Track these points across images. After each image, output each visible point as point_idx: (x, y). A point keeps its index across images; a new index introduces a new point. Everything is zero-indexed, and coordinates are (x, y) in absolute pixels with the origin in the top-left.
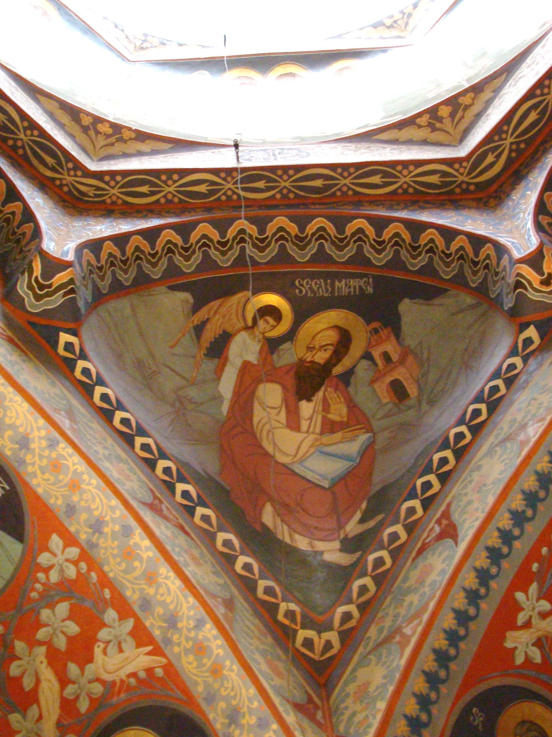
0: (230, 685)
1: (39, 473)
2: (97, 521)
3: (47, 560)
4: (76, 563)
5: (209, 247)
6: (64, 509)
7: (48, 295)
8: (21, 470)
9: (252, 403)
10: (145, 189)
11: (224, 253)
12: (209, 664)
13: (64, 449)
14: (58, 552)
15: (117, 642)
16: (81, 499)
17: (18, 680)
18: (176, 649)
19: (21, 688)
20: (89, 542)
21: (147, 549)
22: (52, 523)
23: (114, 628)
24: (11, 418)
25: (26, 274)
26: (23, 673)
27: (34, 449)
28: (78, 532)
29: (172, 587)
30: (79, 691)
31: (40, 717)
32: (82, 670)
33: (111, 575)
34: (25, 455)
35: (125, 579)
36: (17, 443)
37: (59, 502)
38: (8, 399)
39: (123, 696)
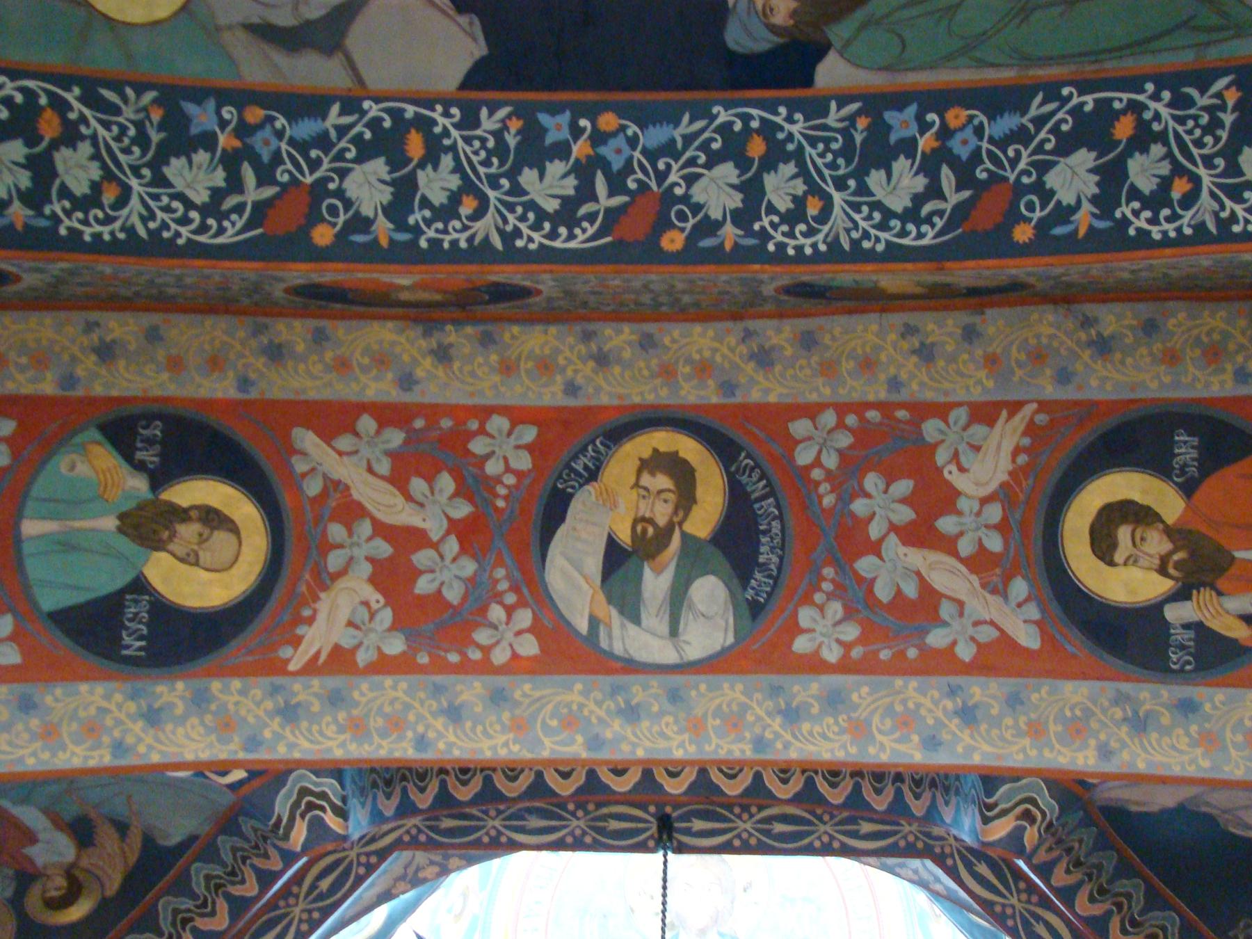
5: (197, 907)
6: (36, 699)
7: (296, 804)
8: (128, 687)
10: (325, 884)
11: (176, 912)
25: (339, 803)
34: (139, 707)
36: (161, 709)
37: (49, 699)
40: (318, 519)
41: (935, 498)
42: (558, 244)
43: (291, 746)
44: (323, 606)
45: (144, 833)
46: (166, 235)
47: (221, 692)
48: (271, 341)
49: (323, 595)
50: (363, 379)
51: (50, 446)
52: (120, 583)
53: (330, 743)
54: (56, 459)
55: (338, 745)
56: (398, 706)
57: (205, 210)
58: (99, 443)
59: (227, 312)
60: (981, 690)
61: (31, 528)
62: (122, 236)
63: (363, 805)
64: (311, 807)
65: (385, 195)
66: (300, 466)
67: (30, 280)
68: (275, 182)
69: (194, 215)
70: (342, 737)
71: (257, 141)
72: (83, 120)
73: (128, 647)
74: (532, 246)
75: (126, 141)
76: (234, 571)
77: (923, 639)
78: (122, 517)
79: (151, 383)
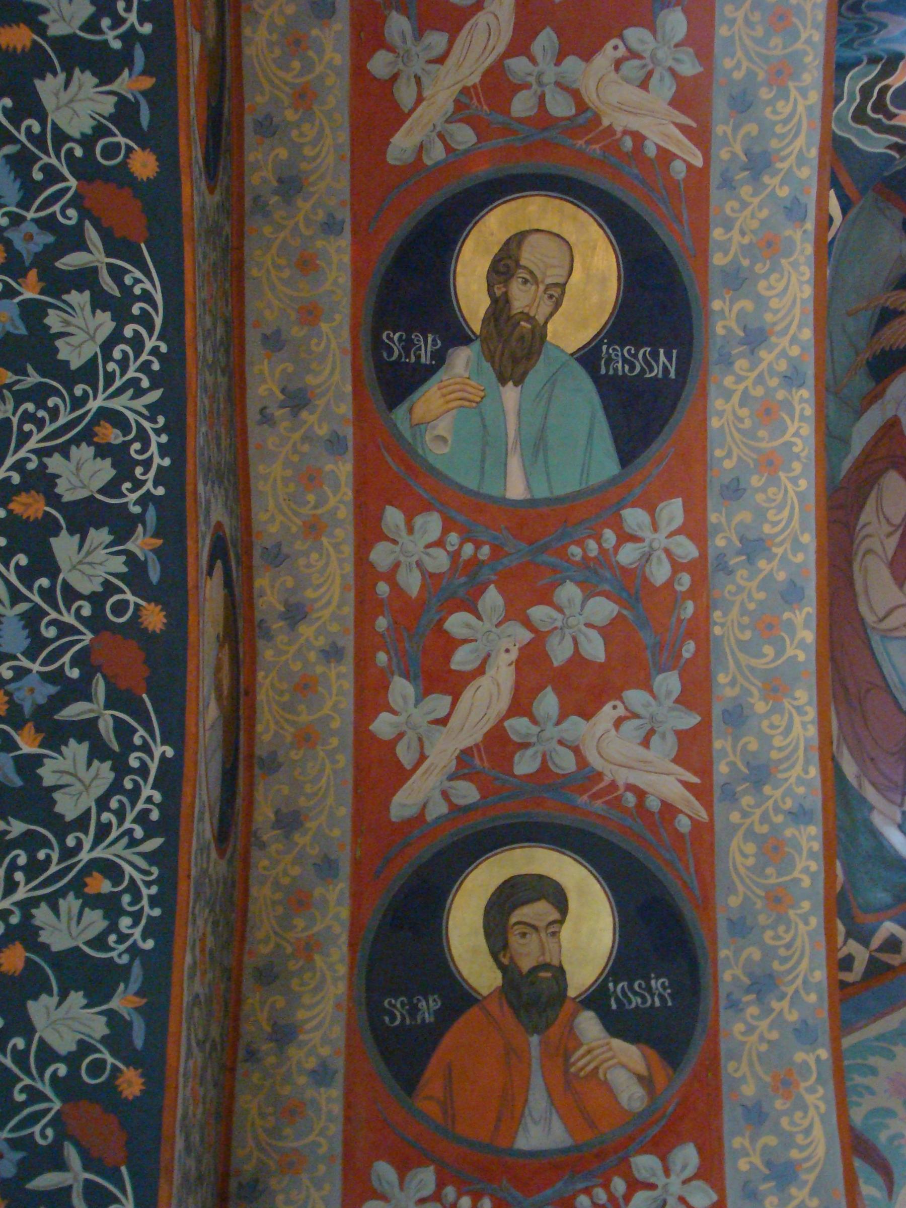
0: (788, 938)
1: (736, 398)
2: (761, 540)
3: (639, 526)
4: (677, 567)
7: (878, 127)
8: (715, 371)
9: (872, 488)
12: (773, 881)
13: (802, 401)
14: (665, 530)
15: (648, 727)
16: (763, 489)
17: (451, 644)
18: (735, 817)
19: (448, 658)
20: (721, 556)
21: (802, 645)
22: (690, 481)
23: (660, 704)
24: (770, 288)
26: (466, 641)
27: (761, 360)
28: (718, 529)
29: (797, 728)
30: (534, 739)
31: (443, 722)
32: (562, 717)
33: (717, 631)
34: (741, 355)
35: (733, 653)
36: (745, 329)
38: (792, 259)
39: (598, 806)
40: (506, 130)
43: (801, 161)
44: (620, 121)
45: (896, 288)
46: (156, 366)
47: (726, 254)
48: (276, 192)
49: (606, 122)
50: (319, 69)
51: (415, 465)
52: (588, 385)
53: (800, 108)
54: (431, 459)
55: (804, 97)
57: (122, 317)
58: (410, 410)
59: (240, 247)
61: (516, 490)
62: (161, 420)
63: (883, 26)
64: (879, 106)
65: (85, 79)
66: (437, 153)
67: (218, 514)
68: (79, 227)
69: (128, 331)
70: (794, 93)
71: (27, 250)
72: (19, 466)
73: (666, 370)
75: (41, 413)
76: (572, 240)
78: (503, 381)
79: (334, 345)
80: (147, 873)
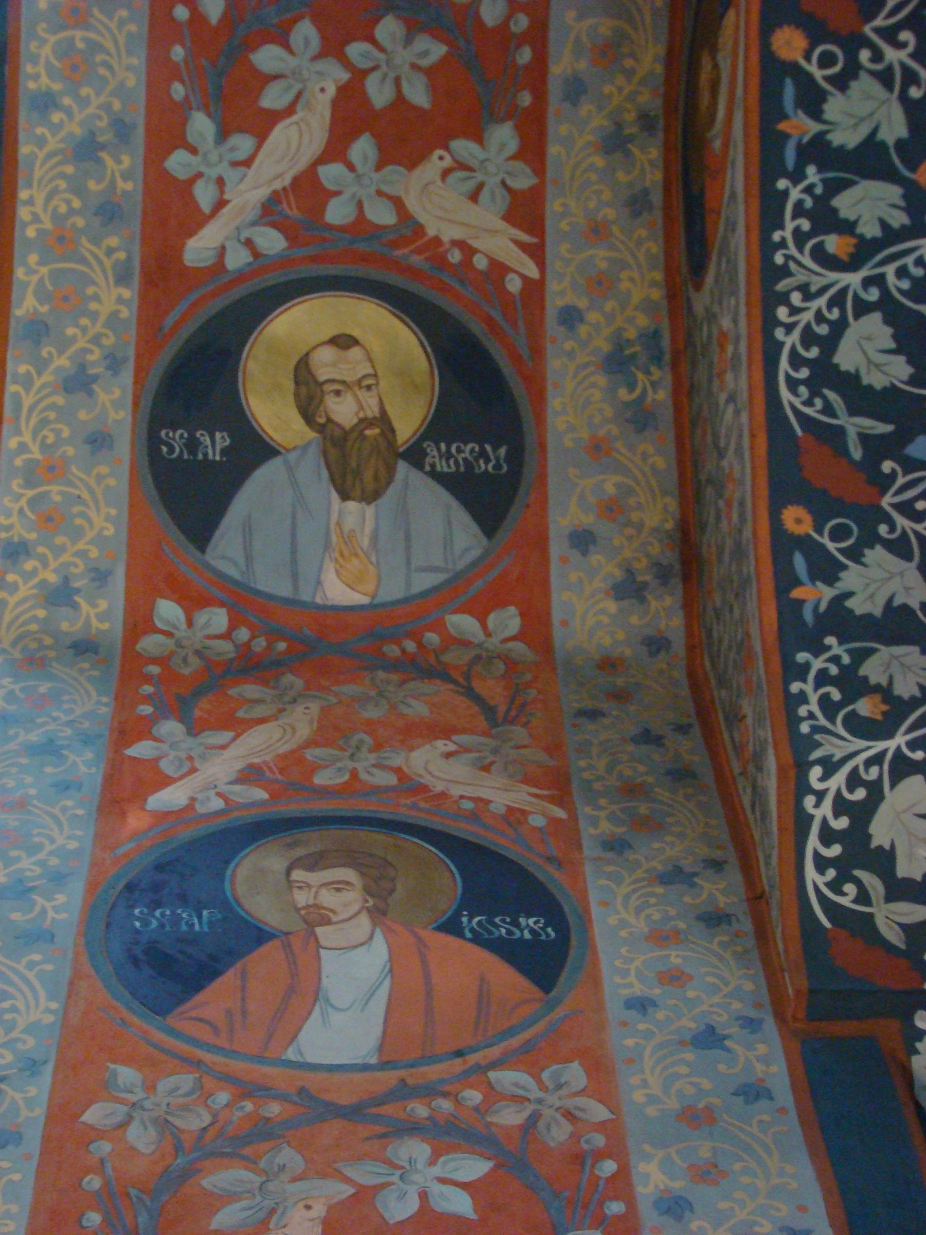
41: (405, 138)
42: (813, 842)
56: (102, 71)
60: (123, 172)
74: (809, 801)
77: (198, 109)
80: (788, 257)
